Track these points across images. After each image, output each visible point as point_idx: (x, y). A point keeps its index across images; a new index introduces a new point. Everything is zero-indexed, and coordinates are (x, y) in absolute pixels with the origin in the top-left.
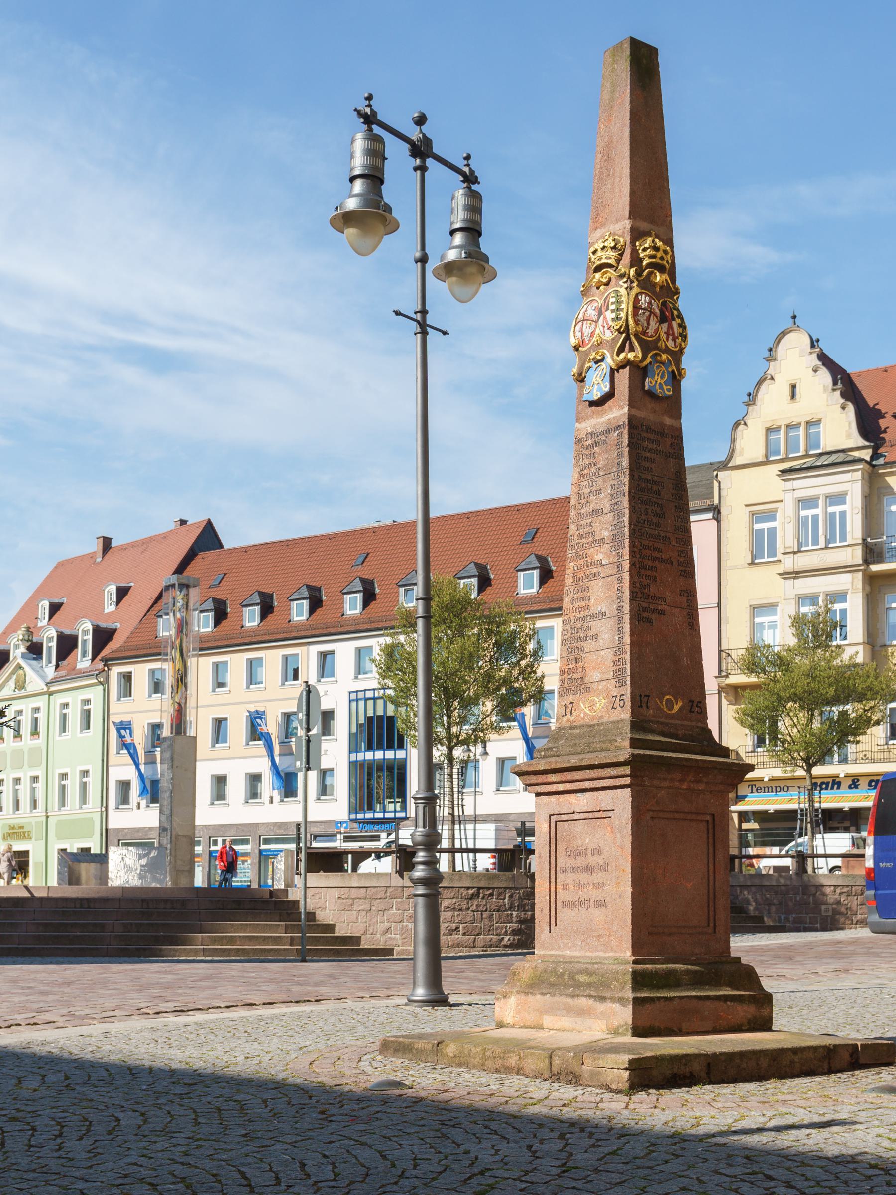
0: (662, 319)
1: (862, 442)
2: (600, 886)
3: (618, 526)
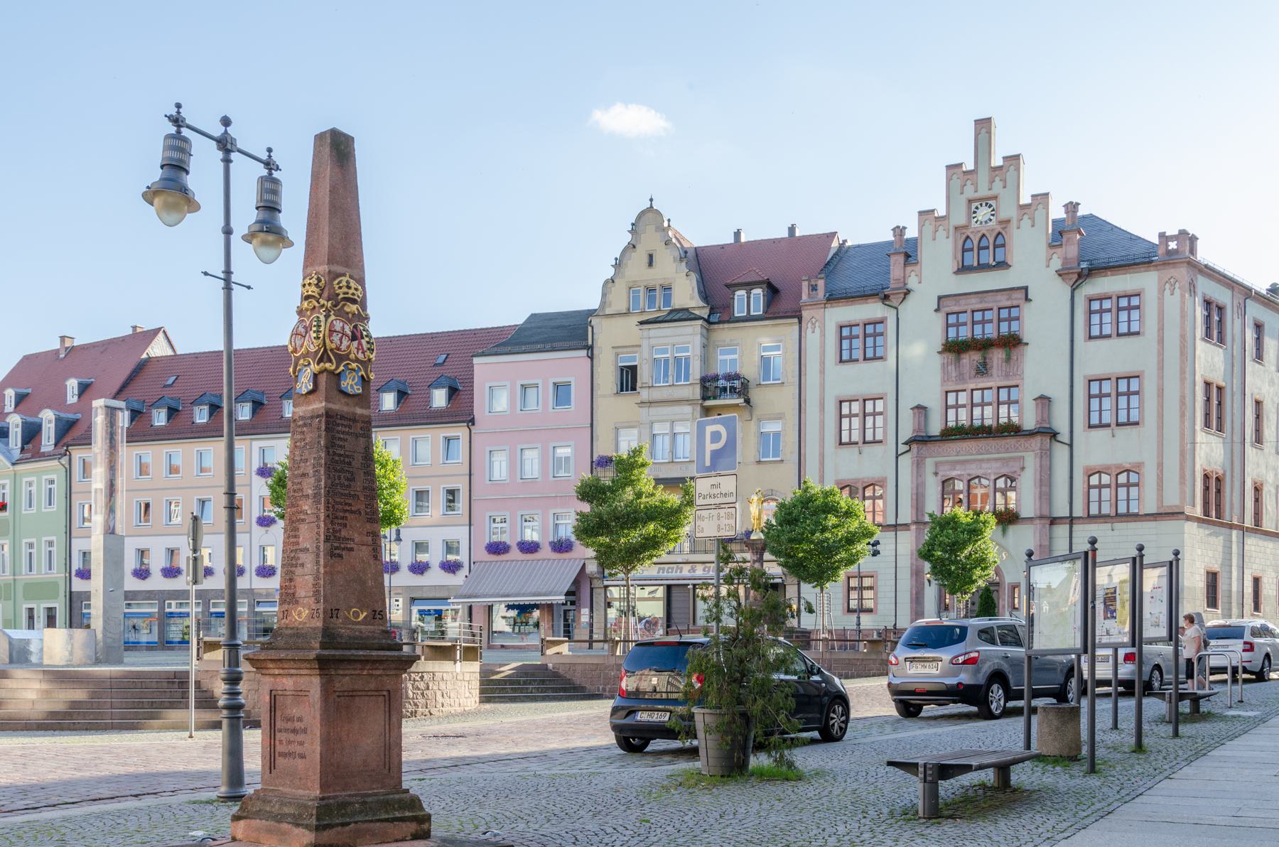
0: (354, 338)
1: (702, 304)
2: (301, 743)
3: (317, 487)
